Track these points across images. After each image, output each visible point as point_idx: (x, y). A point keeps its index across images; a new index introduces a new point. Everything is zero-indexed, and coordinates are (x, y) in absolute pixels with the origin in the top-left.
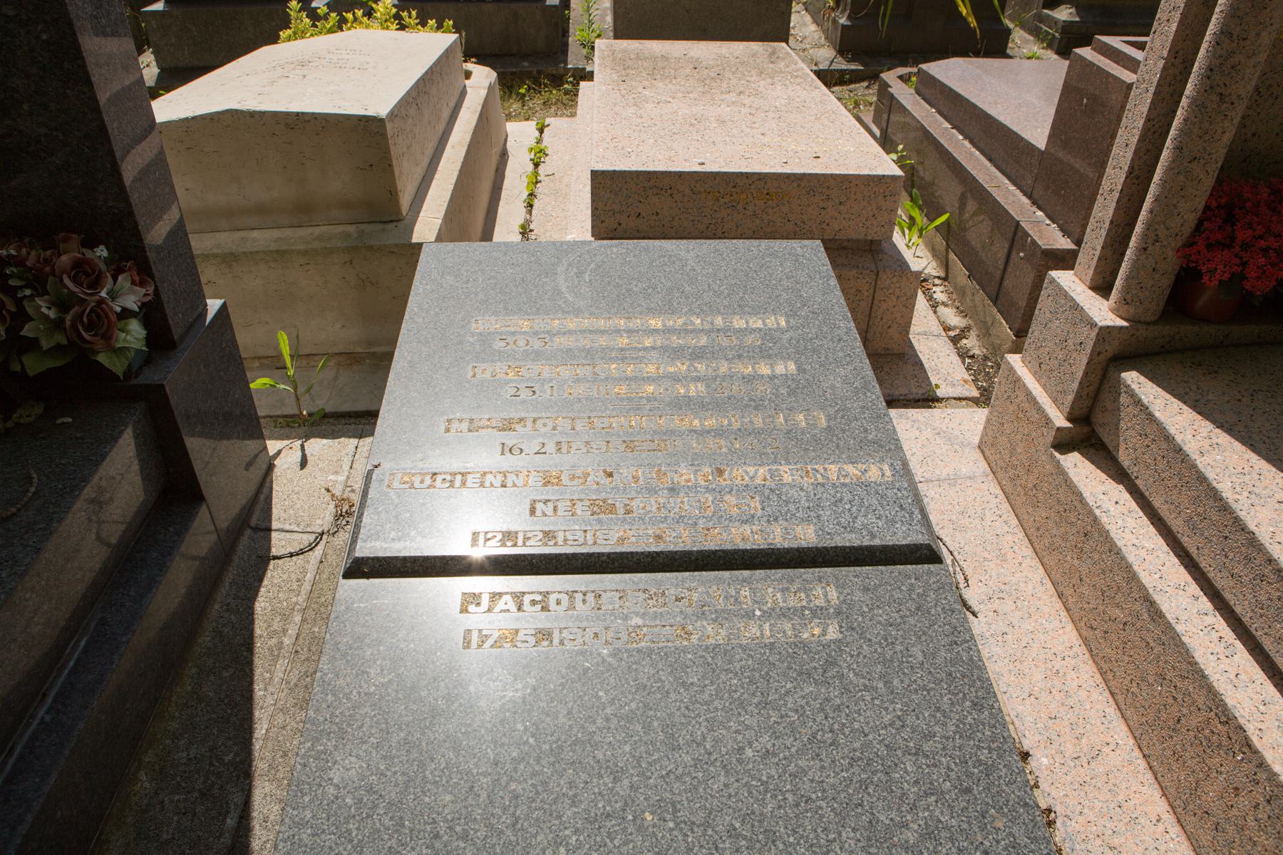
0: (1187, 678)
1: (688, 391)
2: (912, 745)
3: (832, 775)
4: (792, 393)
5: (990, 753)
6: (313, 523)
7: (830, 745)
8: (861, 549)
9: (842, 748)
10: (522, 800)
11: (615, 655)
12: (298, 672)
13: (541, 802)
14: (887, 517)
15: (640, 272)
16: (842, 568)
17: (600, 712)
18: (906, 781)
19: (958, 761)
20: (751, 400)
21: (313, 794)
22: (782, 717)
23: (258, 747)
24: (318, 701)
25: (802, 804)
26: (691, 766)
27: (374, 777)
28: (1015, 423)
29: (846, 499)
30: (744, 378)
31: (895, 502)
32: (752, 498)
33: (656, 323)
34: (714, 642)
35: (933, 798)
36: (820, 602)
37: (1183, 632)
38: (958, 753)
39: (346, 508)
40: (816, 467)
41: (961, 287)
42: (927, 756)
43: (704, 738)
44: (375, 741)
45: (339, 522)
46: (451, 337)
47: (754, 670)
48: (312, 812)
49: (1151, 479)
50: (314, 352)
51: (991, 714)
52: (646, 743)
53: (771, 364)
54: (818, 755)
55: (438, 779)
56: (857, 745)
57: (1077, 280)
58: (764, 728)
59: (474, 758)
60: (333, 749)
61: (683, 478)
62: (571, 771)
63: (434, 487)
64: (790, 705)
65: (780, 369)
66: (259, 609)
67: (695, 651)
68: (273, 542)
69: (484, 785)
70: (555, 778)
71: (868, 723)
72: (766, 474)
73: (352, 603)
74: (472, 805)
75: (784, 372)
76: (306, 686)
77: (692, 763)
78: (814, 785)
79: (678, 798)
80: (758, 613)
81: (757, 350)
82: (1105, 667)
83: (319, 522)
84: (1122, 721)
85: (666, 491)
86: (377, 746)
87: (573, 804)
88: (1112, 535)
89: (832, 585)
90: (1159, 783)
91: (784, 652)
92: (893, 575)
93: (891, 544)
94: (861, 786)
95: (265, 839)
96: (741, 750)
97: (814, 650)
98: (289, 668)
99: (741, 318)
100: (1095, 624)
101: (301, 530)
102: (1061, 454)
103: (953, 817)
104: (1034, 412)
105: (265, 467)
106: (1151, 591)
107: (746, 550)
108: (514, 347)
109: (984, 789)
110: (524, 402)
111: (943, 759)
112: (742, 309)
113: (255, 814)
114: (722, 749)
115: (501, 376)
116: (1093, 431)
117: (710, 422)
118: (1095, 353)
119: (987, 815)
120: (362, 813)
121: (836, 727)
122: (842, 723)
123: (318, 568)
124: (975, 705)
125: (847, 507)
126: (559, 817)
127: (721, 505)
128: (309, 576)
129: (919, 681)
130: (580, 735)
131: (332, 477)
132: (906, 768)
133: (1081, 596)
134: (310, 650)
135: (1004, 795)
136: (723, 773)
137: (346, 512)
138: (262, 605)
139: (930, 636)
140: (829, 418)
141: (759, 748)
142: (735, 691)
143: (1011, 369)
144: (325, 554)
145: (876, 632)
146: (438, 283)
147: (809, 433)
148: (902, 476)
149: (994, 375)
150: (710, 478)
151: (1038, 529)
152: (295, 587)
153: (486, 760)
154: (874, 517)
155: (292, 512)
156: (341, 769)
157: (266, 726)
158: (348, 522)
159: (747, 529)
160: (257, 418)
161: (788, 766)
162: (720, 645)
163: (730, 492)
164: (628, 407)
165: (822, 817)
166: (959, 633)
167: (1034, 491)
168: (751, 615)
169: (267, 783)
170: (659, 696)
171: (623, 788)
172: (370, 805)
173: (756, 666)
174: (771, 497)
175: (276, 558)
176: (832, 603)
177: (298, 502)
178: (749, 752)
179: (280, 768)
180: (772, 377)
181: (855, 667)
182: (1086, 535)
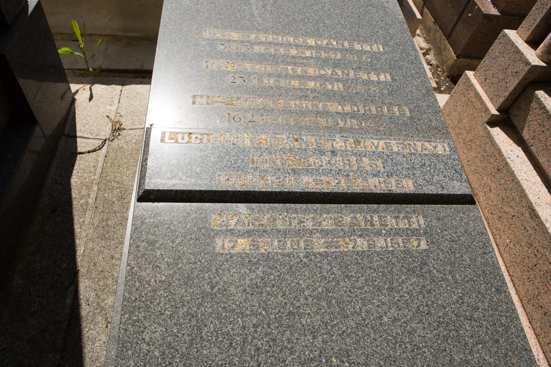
0: (547, 248)
1: (333, 87)
2: (468, 314)
3: (429, 332)
4: (390, 93)
5: (506, 319)
7: (427, 314)
8: (437, 195)
9: (433, 316)
10: (261, 351)
11: (307, 257)
12: (98, 219)
13: (273, 352)
14: (449, 176)
15: (299, 8)
16: (425, 205)
17: (302, 294)
18: (467, 336)
19: (491, 324)
20: (368, 96)
21: (133, 349)
22: (401, 297)
24: (130, 286)
25: (415, 350)
26: (355, 328)
27: (171, 338)
28: (465, 107)
29: (427, 164)
30: (363, 82)
31: (452, 168)
32: (378, 160)
33: (311, 42)
34: (361, 249)
35: (481, 346)
36: (415, 226)
37: (549, 227)
38: (491, 319)
39: (118, 126)
40: (410, 142)
41: (428, 27)
42: (476, 321)
43: (361, 310)
44: (169, 313)
45: (114, 134)
46: (191, 40)
47: (384, 268)
48: (134, 361)
49: (541, 148)
50: (94, 33)
51: (505, 295)
52: (329, 313)
54: (421, 321)
55: (210, 338)
56: (441, 314)
57: (518, 37)
58: (392, 304)
59: (231, 324)
60: (143, 319)
61: (338, 145)
62: (288, 332)
63: (191, 142)
64: (405, 290)
65: (382, 78)
66: (74, 182)
67: (352, 255)
68: (78, 144)
69: (239, 342)
70: (279, 336)
71: (445, 301)
72: (384, 145)
73: (145, 219)
74: (232, 355)
75: (384, 80)
76: (103, 227)
77: (355, 326)
78: (420, 339)
79: (349, 348)
80: (384, 232)
81: (369, 65)
82: (496, 232)
83: (103, 133)
85: (329, 153)
86: (171, 317)
87: (292, 353)
88: (516, 173)
89: (421, 215)
90: (515, 288)
91: (399, 257)
92: (451, 211)
93: (452, 193)
94: (444, 338)
95: (89, 311)
96: (381, 317)
97: (415, 256)
99: (358, 44)
100: (494, 212)
101: (93, 138)
102: (491, 127)
103: (491, 357)
104: (479, 104)
105: (70, 99)
106: (534, 205)
107: (377, 194)
109: (505, 340)
110: (239, 86)
111: (484, 323)
112: (358, 38)
113: (81, 297)
114: (371, 317)
115: (223, 68)
116: (509, 117)
117: (347, 108)
118: (524, 78)
119: (508, 356)
120: (166, 361)
121: (429, 303)
122: (432, 301)
124: (497, 290)
126: (284, 361)
127: (361, 164)
128: (100, 164)
129: (469, 276)
130: (291, 309)
131: (109, 107)
132: (466, 328)
133: (489, 198)
134: (104, 207)
135: (515, 344)
136: (372, 332)
137: (118, 128)
138: (75, 180)
139: (473, 249)
140: (411, 111)
141: (390, 316)
142: (376, 281)
143: (468, 79)
144: (108, 152)
145: (445, 245)
146: (179, 3)
147: (401, 119)
148: (454, 152)
150: (354, 145)
151: (469, 161)
152: (92, 170)
153: (238, 326)
154: (442, 176)
155: (87, 127)
156: (149, 332)
157: (83, 249)
158: (119, 134)
159: (376, 180)
160: (64, 69)
161: (406, 327)
162: (365, 251)
163: (365, 156)
164: (300, 95)
165: (426, 358)
166: (487, 247)
167: (470, 143)
168: (380, 233)
169: (86, 280)
170: (334, 283)
171: (318, 342)
172: (170, 356)
173: (385, 265)
174: (388, 160)
175: (80, 153)
176: (422, 227)
178: (385, 319)
179: (93, 272)
180: (379, 83)
181: (436, 266)
182: (498, 170)
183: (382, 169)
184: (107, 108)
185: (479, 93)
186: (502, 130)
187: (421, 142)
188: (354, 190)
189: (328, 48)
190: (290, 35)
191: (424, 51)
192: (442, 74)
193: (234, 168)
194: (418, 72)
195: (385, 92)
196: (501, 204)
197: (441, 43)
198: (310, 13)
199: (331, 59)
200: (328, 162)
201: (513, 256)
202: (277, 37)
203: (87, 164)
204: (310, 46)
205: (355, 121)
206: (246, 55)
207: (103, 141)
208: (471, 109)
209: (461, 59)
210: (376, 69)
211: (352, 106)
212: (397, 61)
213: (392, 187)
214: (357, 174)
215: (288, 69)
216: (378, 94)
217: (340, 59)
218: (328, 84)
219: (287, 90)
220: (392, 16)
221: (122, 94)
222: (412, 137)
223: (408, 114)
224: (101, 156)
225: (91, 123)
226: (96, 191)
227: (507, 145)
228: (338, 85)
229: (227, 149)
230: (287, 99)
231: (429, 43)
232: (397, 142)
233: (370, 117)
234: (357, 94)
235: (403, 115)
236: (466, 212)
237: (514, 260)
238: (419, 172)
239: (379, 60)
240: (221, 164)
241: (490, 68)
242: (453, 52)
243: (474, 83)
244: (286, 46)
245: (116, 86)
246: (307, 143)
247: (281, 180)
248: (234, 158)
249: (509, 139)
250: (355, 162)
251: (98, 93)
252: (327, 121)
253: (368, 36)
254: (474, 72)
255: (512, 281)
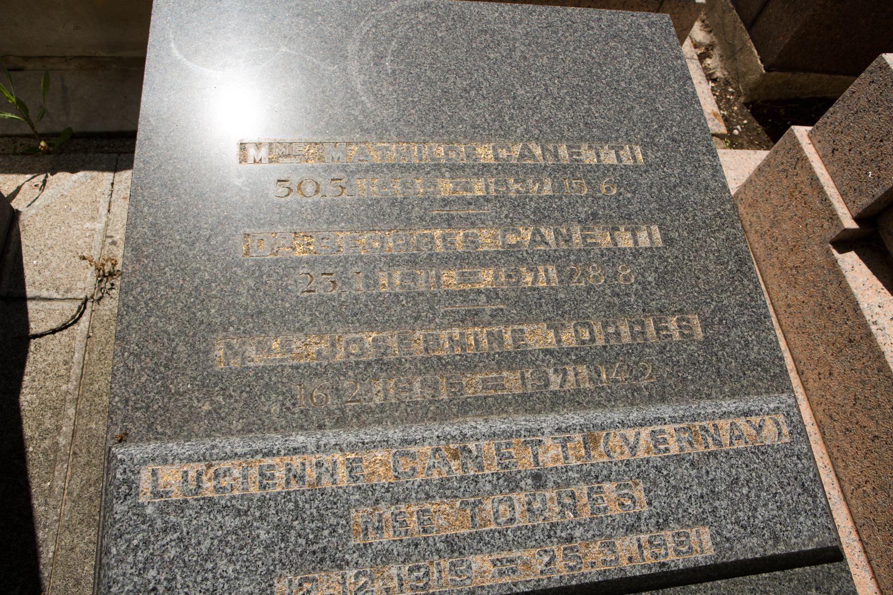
4: (662, 282)
6: (74, 287)
12: (79, 480)
14: (789, 505)
16: (736, 579)
23: (46, 575)
28: (787, 199)
29: (742, 477)
30: (602, 255)
31: (796, 479)
33: (485, 153)
40: (704, 423)
45: (103, 286)
50: (48, 54)
53: (633, 231)
61: (549, 455)
65: (643, 238)
66: (25, 404)
76: (90, 498)
82: (836, 454)
83: (80, 285)
84: (843, 503)
85: (529, 481)
90: (872, 568)
92: (792, 585)
98: (69, 473)
99: (590, 147)
101: (59, 297)
102: (840, 252)
108: (299, 197)
123: (86, 345)
125: (744, 492)
127: (600, 501)
131: (88, 225)
134: (89, 452)
138: (28, 397)
144: (92, 327)
149: (734, 103)
150: (583, 451)
152: (63, 372)
154: (775, 507)
155: (47, 273)
157: (52, 548)
158: (112, 285)
163: (608, 478)
167: (794, 272)
175: (35, 336)
177: (54, 260)
180: (637, 253)
183: (646, 508)
184: (85, 226)
185: (818, 179)
186: (860, 258)
187: (729, 417)
188: (585, 578)
189: (524, 166)
190: (437, 138)
191: (702, 50)
192: (736, 100)
193: (314, 552)
194: (719, 213)
195: (650, 279)
196: (851, 407)
197: (734, 35)
198: (481, 71)
199: (531, 199)
200: (526, 507)
201: (871, 509)
202: (408, 148)
203: (50, 358)
204: (484, 166)
205: (583, 369)
206: (338, 206)
207: (79, 303)
208: (800, 207)
209: (773, 74)
210: (629, 217)
211: (579, 328)
212: (675, 186)
213: (667, 554)
214: (591, 532)
215: (433, 238)
216: (634, 287)
217: (550, 197)
218: (524, 269)
219: (433, 300)
220: (660, 63)
221: (115, 192)
222: (708, 396)
223: (699, 334)
224: (78, 338)
225: (54, 265)
226: (73, 417)
227: (870, 292)
228: (546, 271)
229: (296, 502)
230: (432, 326)
231: (711, 32)
232: (677, 426)
233: (618, 354)
234: (588, 293)
235: (688, 337)
236: (823, 584)
237: (872, 517)
238: (724, 504)
239: (636, 189)
240: (283, 545)
241: (846, 130)
242: (758, 57)
243: (809, 156)
244: (429, 173)
245: (100, 174)
246: (479, 459)
247: (421, 574)
248: (313, 526)
249: (874, 277)
250: (585, 500)
251: (66, 193)
252: (523, 378)
253: (611, 123)
254: (809, 128)
255: (865, 552)
